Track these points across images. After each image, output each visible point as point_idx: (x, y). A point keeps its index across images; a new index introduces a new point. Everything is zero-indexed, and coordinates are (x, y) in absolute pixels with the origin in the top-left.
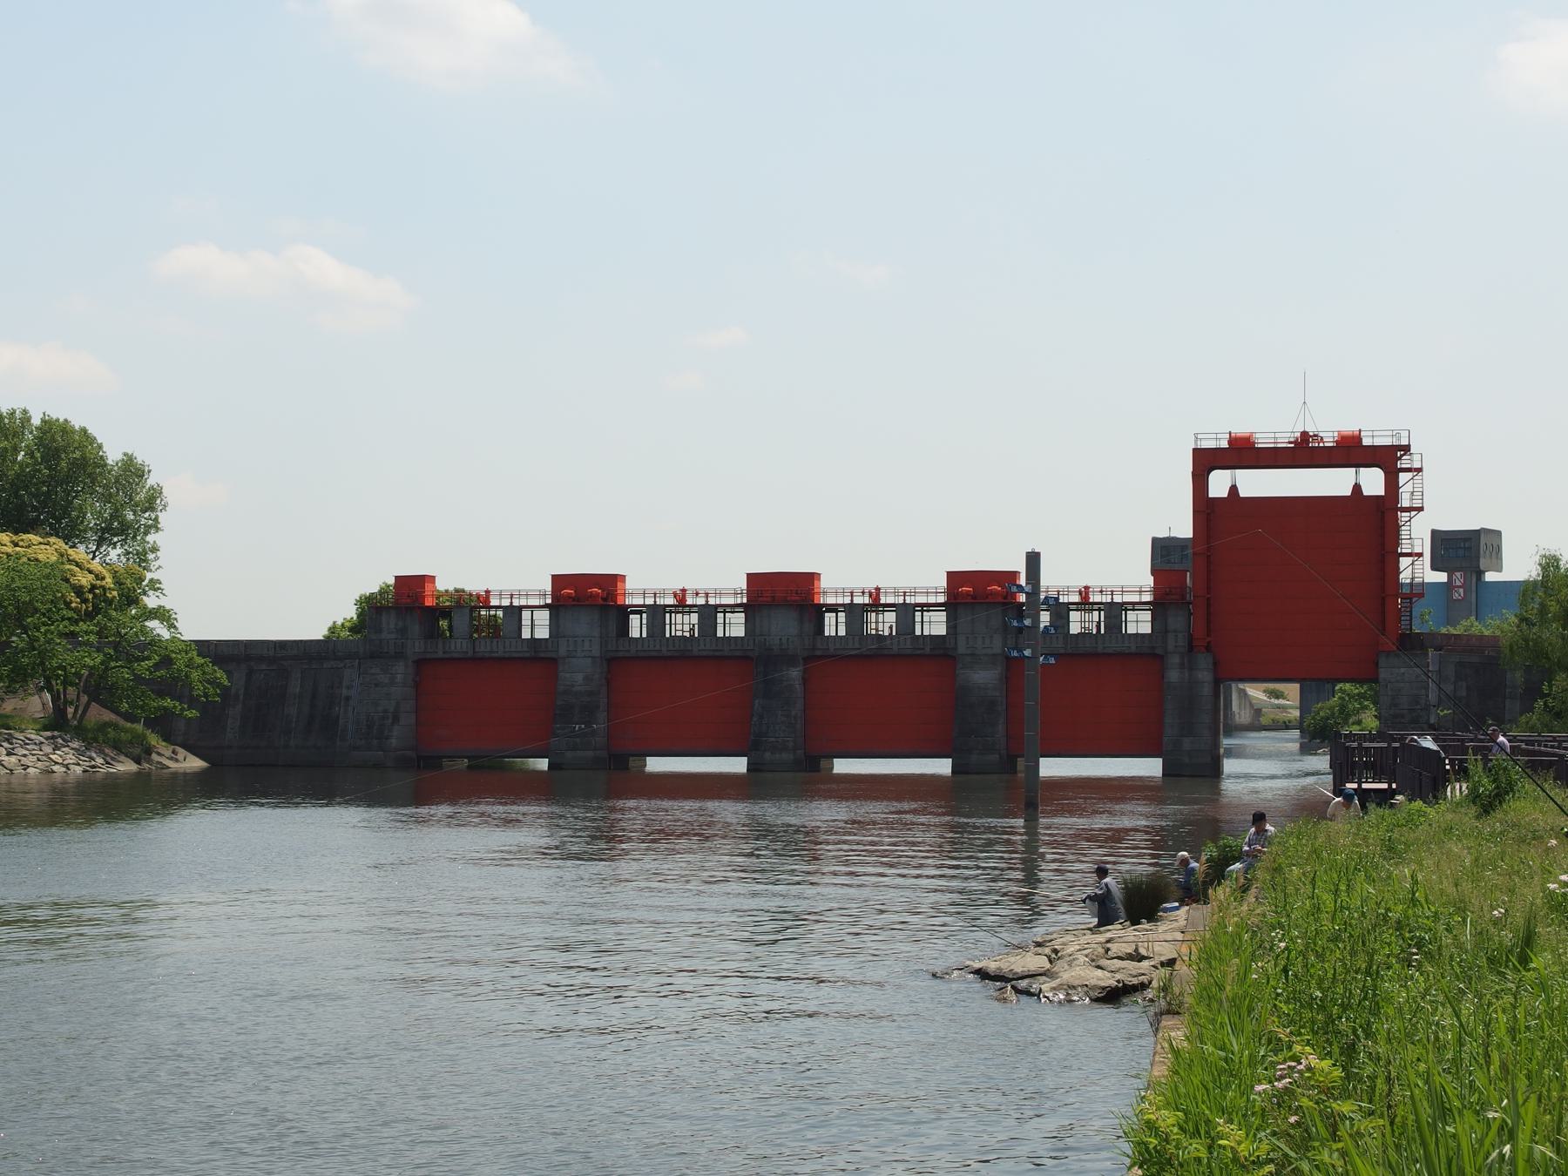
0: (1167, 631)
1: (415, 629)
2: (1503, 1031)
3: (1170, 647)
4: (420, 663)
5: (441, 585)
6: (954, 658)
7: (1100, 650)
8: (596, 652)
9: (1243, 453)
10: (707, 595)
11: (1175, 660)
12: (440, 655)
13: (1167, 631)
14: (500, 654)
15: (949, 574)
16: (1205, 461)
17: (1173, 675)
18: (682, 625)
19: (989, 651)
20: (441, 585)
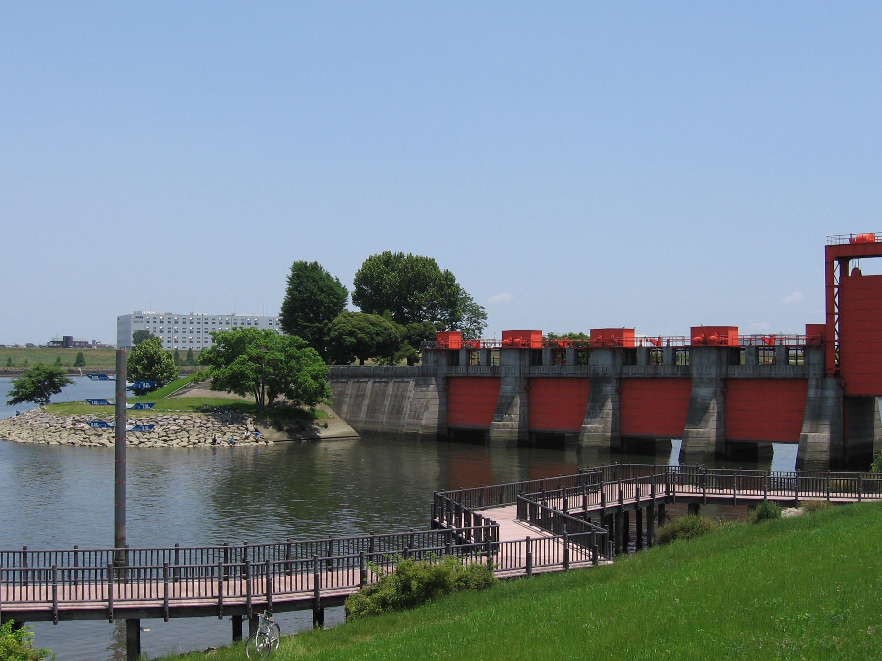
0: (809, 364)
1: (444, 361)
2: (440, 564)
3: (811, 375)
4: (448, 379)
5: (741, 333)
6: (500, 378)
7: (773, 375)
8: (518, 375)
9: (867, 247)
10: (668, 341)
11: (813, 383)
12: (454, 374)
13: (809, 364)
14: (662, 375)
15: (808, 326)
16: (838, 255)
17: (812, 393)
18: (767, 358)
19: (709, 376)
20: (741, 333)
